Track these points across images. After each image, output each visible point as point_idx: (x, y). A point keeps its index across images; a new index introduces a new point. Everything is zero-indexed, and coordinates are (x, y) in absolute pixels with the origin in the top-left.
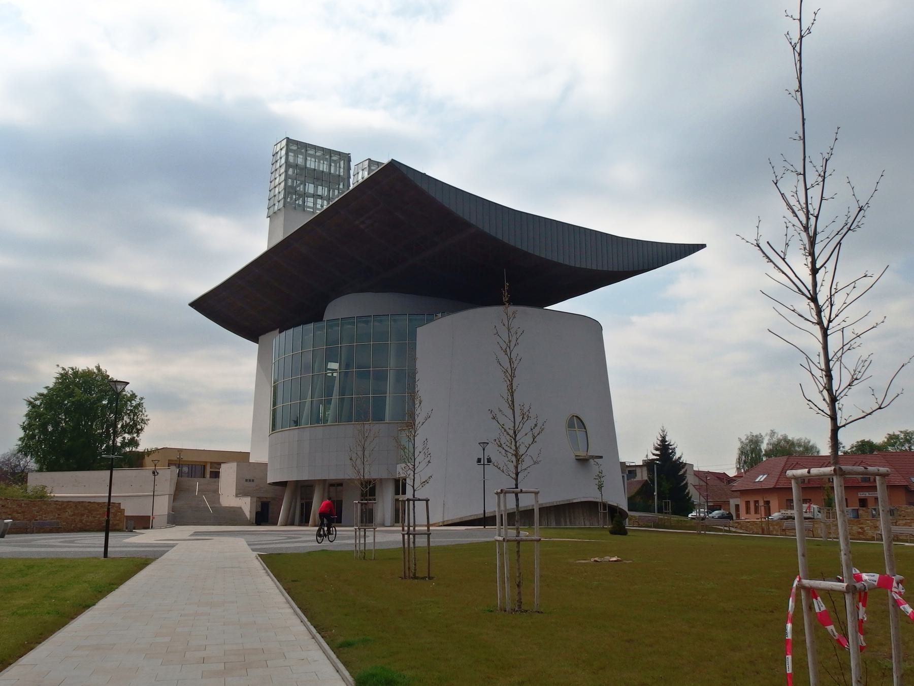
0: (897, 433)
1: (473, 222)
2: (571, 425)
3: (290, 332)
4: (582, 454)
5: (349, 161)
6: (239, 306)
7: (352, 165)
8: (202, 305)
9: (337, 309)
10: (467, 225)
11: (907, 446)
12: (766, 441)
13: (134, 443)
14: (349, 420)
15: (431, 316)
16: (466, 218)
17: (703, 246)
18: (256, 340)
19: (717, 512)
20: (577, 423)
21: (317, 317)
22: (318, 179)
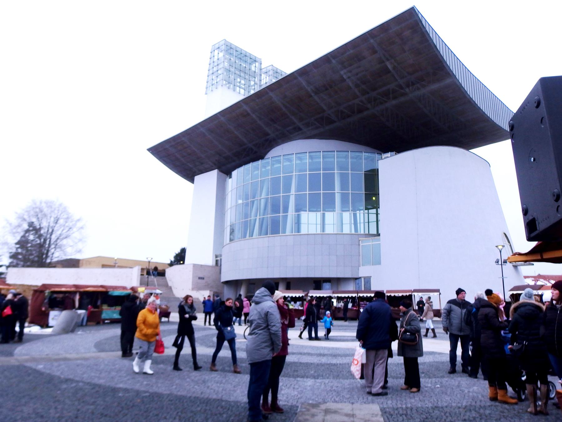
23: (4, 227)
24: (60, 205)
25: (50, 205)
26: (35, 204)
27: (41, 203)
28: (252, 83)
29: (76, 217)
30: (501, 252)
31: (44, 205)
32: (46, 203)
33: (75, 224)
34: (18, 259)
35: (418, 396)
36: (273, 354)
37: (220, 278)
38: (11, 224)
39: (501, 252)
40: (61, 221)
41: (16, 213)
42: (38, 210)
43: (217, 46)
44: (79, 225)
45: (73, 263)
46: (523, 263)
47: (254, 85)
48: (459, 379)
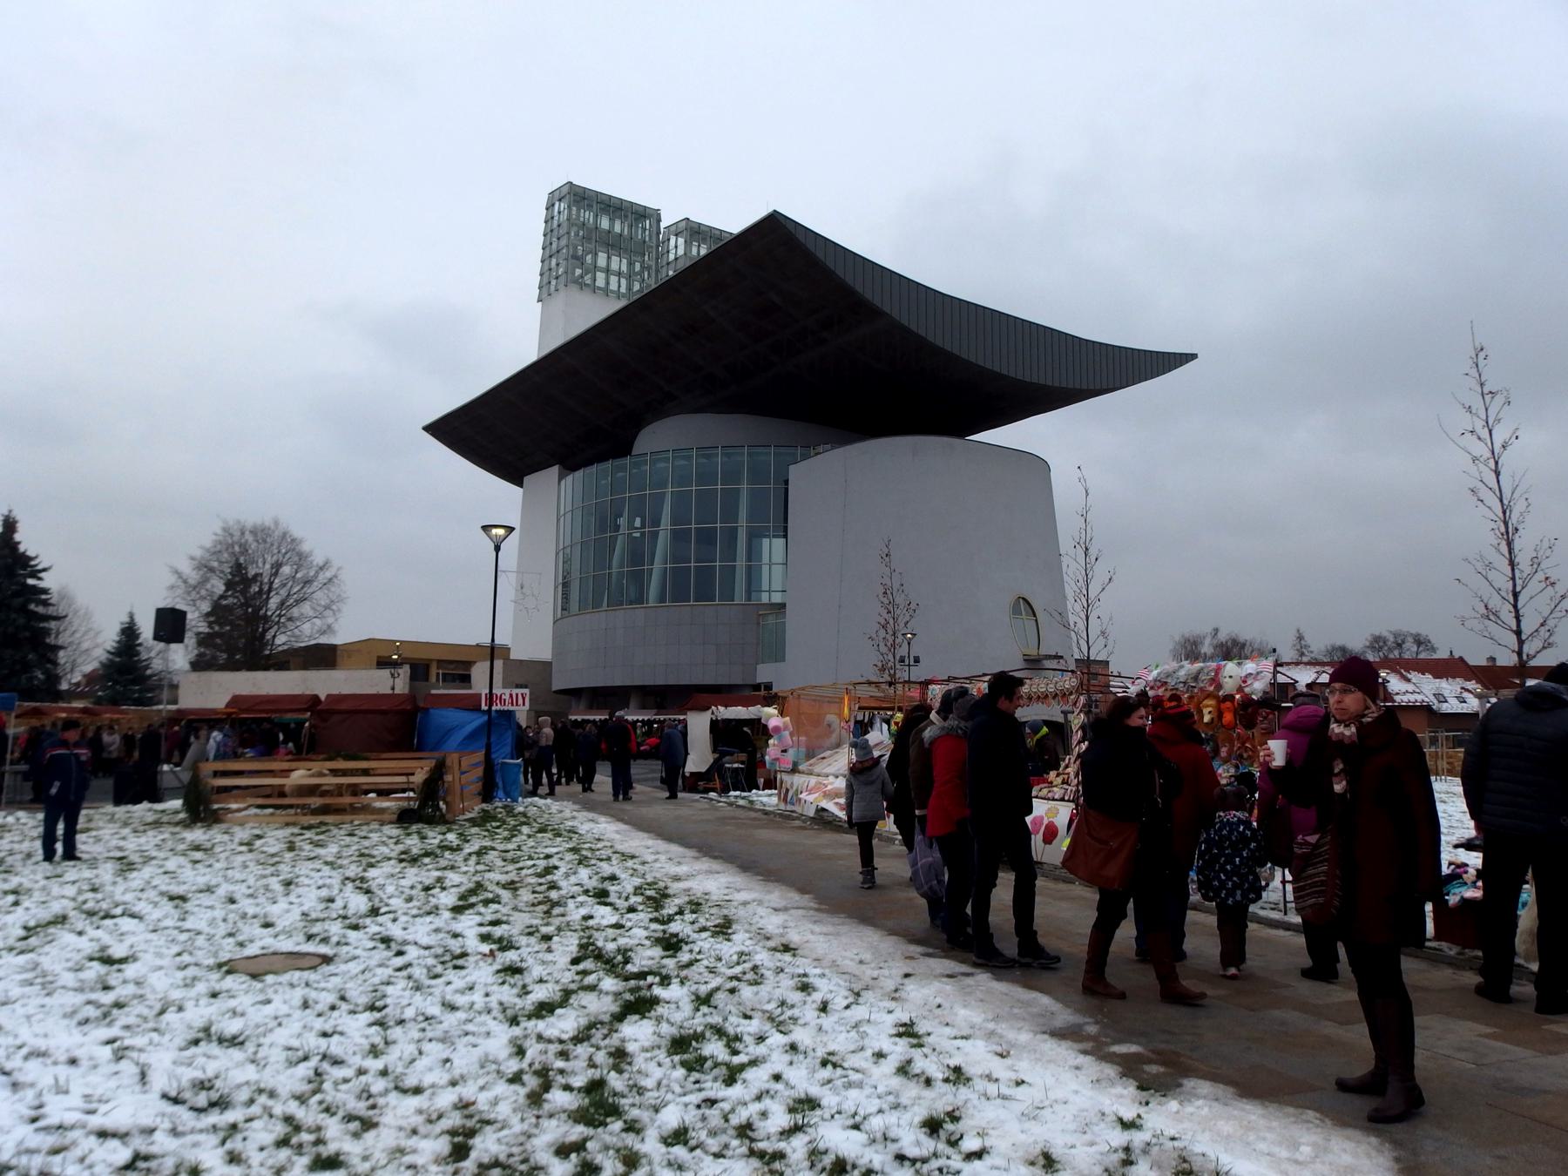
0: (1385, 634)
1: (887, 309)
2: (1016, 610)
3: (579, 474)
4: (1033, 652)
5: (659, 221)
6: (495, 431)
7: (663, 225)
8: (427, 429)
9: (655, 439)
10: (875, 313)
11: (1396, 653)
12: (1207, 641)
13: (329, 629)
14: (597, 605)
15: (809, 448)
16: (877, 302)
17: (1193, 356)
18: (520, 484)
19: (630, 718)
20: (1024, 606)
21: (620, 447)
22: (613, 246)
23: (172, 587)
24: (285, 534)
25: (261, 533)
26: (232, 535)
27: (243, 533)
28: (638, 267)
29: (318, 559)
30: (497, 549)
31: (249, 537)
32: (254, 532)
33: (316, 576)
34: (215, 646)
35: (918, 1120)
36: (1218, 670)
37: (550, 684)
38: (185, 582)
39: (497, 549)
40: (286, 570)
41: (193, 558)
42: (237, 548)
43: (557, 195)
44: (323, 577)
45: (323, 657)
46: (270, 810)
47: (641, 273)
48: (1065, 1052)
